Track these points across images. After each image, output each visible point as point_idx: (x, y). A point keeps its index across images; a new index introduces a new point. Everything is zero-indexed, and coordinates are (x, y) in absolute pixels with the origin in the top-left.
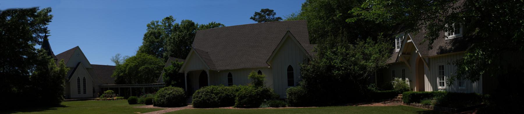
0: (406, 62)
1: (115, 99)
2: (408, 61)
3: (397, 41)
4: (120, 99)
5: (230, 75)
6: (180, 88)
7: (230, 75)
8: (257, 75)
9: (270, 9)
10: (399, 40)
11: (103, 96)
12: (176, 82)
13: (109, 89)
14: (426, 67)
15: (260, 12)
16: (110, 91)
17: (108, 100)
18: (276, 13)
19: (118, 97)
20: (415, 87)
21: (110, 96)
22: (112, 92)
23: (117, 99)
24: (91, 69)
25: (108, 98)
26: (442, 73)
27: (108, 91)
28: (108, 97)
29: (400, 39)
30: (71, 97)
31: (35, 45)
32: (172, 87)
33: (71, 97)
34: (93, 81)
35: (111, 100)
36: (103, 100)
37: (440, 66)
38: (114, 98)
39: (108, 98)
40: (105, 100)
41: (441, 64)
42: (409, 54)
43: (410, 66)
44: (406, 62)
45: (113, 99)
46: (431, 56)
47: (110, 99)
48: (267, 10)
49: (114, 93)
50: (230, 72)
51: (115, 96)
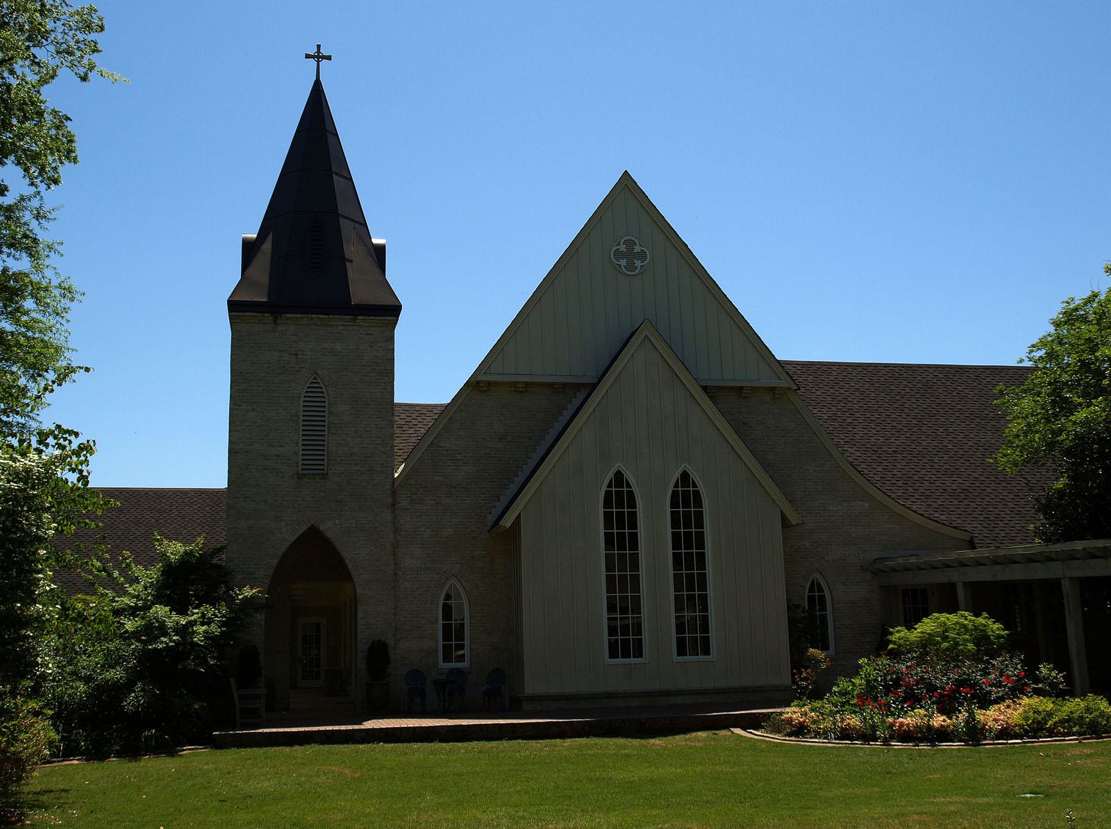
1: (1005, 733)
4: (1068, 726)
8: (830, 651)
11: (870, 686)
13: (961, 593)
16: (964, 618)
17: (906, 736)
19: (1047, 704)
21: (945, 681)
22: (982, 638)
23: (1036, 728)
24: (773, 389)
25: (912, 719)
27: (927, 625)
28: (913, 700)
30: (532, 686)
31: (20, 778)
33: (532, 686)
34: (785, 523)
35: (943, 735)
36: (846, 734)
38: (980, 715)
39: (912, 719)
40: (867, 736)
45: (974, 734)
47: (939, 720)
49: (1012, 645)
50: (610, 658)
51: (1016, 691)
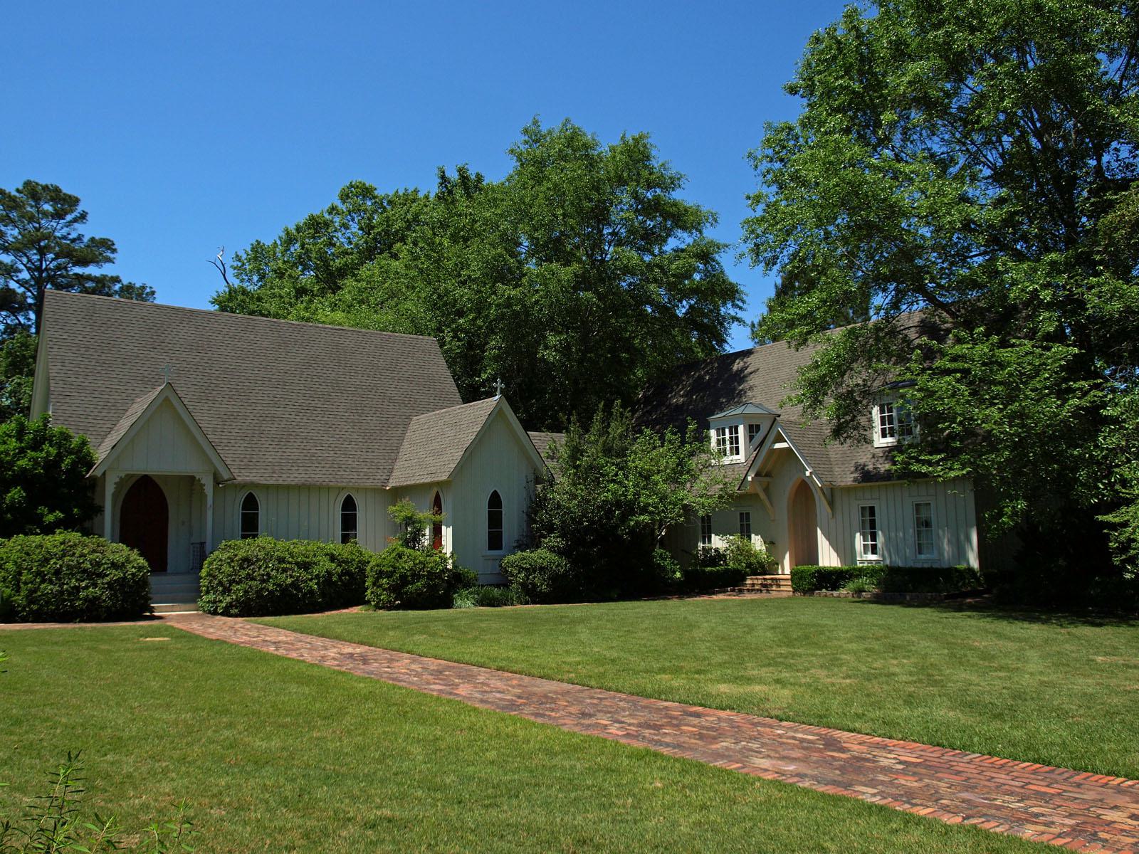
0: (762, 496)
2: (766, 490)
3: (718, 435)
5: (250, 503)
6: (127, 546)
7: (349, 504)
9: (66, 189)
10: (724, 434)
12: (61, 515)
14: (822, 506)
15: (18, 191)
18: (88, 217)
20: (785, 553)
26: (868, 525)
29: (727, 431)
32: (83, 536)
37: (741, 514)
41: (868, 504)
42: (768, 475)
43: (771, 504)
44: (762, 496)
46: (843, 484)
48: (55, 194)
50: (250, 493)
